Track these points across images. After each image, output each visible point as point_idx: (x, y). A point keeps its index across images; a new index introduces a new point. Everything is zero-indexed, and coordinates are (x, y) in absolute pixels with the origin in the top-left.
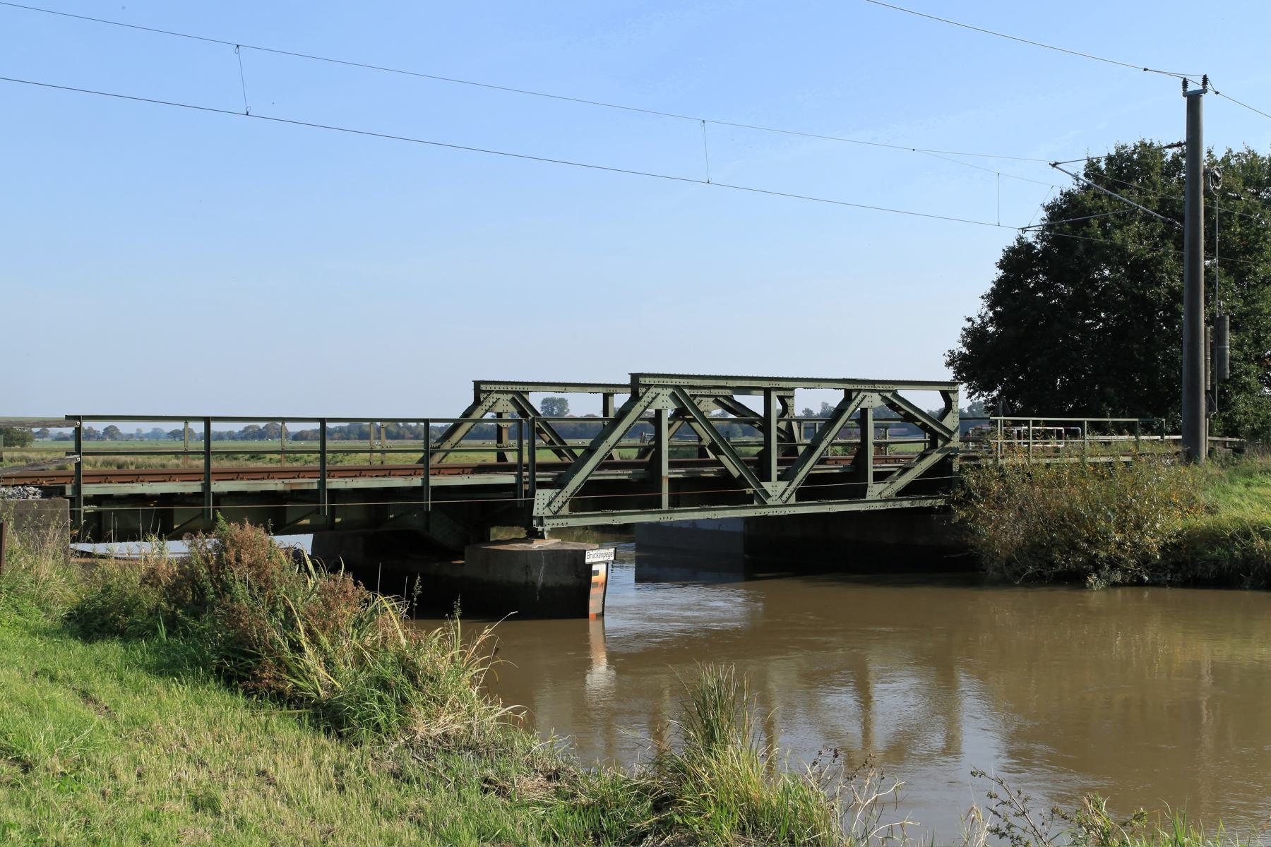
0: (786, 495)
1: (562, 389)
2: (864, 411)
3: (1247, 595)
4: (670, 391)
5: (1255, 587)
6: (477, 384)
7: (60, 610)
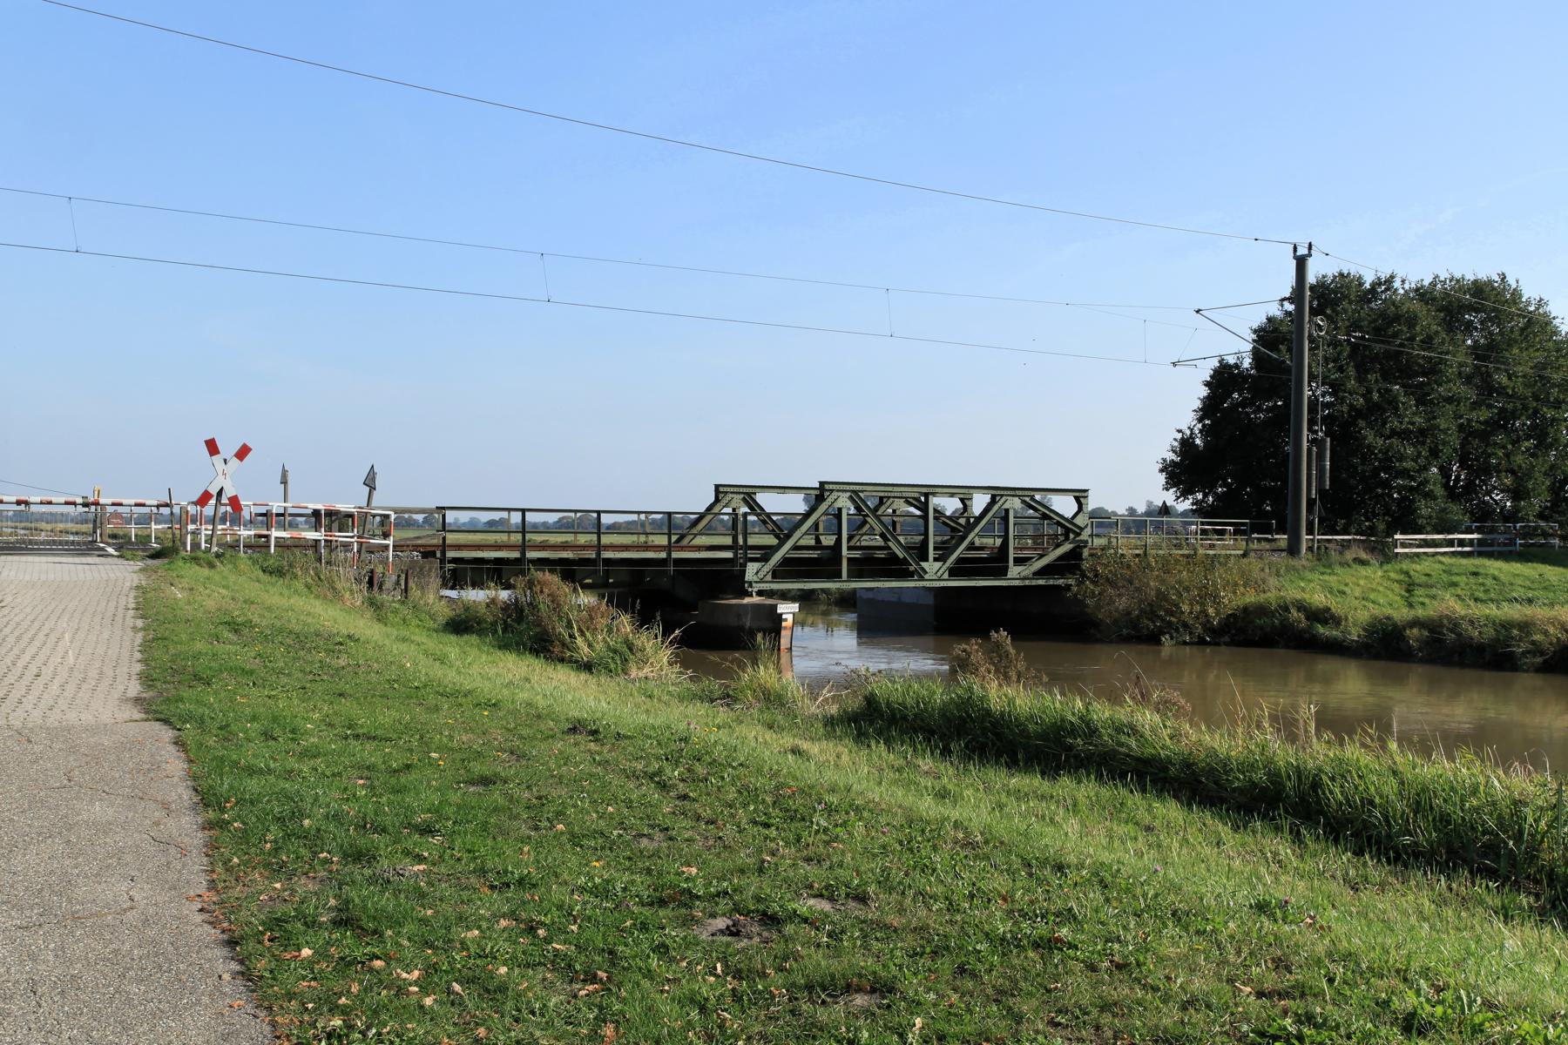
0: (941, 572)
1: (782, 491)
2: (1007, 511)
3: (1282, 652)
4: (848, 494)
5: (1287, 647)
6: (717, 487)
7: (442, 620)
